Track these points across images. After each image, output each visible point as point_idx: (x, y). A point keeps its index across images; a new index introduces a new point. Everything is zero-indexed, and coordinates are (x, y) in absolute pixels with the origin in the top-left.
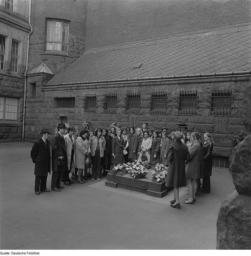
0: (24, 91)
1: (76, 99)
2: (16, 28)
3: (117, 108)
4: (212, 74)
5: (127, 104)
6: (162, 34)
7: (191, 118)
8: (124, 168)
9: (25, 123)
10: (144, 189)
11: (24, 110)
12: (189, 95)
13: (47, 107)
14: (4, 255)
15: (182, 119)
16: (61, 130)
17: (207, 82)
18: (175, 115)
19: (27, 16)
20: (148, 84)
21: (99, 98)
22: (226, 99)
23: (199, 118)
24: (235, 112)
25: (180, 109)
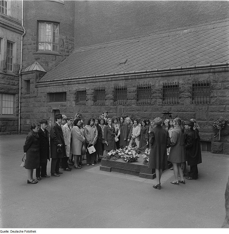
0: (19, 88)
1: (68, 93)
2: (10, 30)
3: (106, 100)
4: (192, 67)
5: (115, 96)
6: (144, 32)
7: (174, 108)
8: (117, 153)
9: (20, 117)
10: (137, 172)
11: (20, 105)
12: (171, 86)
13: (41, 102)
14: (4, 233)
15: (166, 108)
16: (59, 120)
17: (188, 74)
18: (159, 105)
19: (20, 19)
20: (133, 77)
21: (88, 92)
22: (205, 90)
23: (182, 107)
24: (214, 101)
25: (164, 99)
